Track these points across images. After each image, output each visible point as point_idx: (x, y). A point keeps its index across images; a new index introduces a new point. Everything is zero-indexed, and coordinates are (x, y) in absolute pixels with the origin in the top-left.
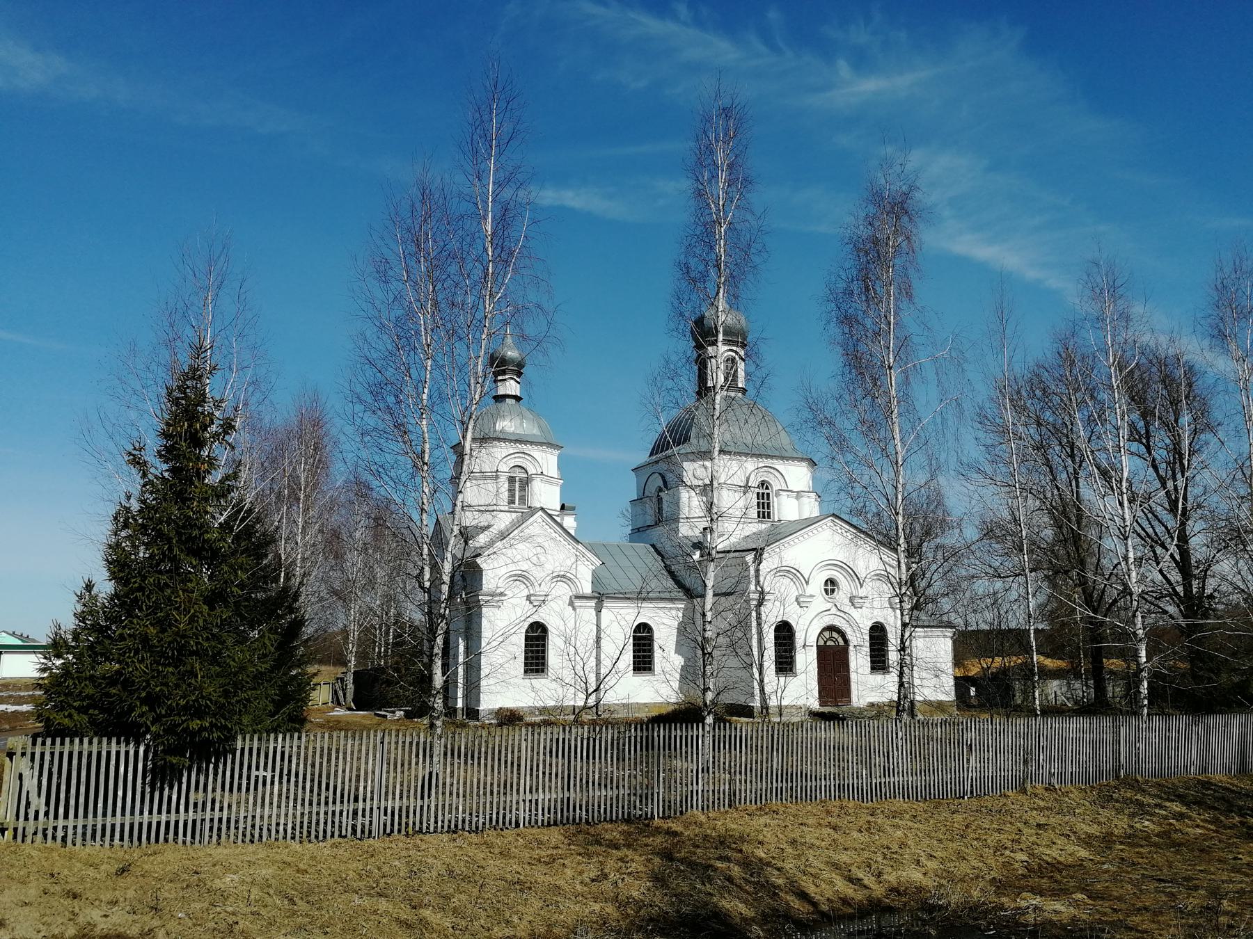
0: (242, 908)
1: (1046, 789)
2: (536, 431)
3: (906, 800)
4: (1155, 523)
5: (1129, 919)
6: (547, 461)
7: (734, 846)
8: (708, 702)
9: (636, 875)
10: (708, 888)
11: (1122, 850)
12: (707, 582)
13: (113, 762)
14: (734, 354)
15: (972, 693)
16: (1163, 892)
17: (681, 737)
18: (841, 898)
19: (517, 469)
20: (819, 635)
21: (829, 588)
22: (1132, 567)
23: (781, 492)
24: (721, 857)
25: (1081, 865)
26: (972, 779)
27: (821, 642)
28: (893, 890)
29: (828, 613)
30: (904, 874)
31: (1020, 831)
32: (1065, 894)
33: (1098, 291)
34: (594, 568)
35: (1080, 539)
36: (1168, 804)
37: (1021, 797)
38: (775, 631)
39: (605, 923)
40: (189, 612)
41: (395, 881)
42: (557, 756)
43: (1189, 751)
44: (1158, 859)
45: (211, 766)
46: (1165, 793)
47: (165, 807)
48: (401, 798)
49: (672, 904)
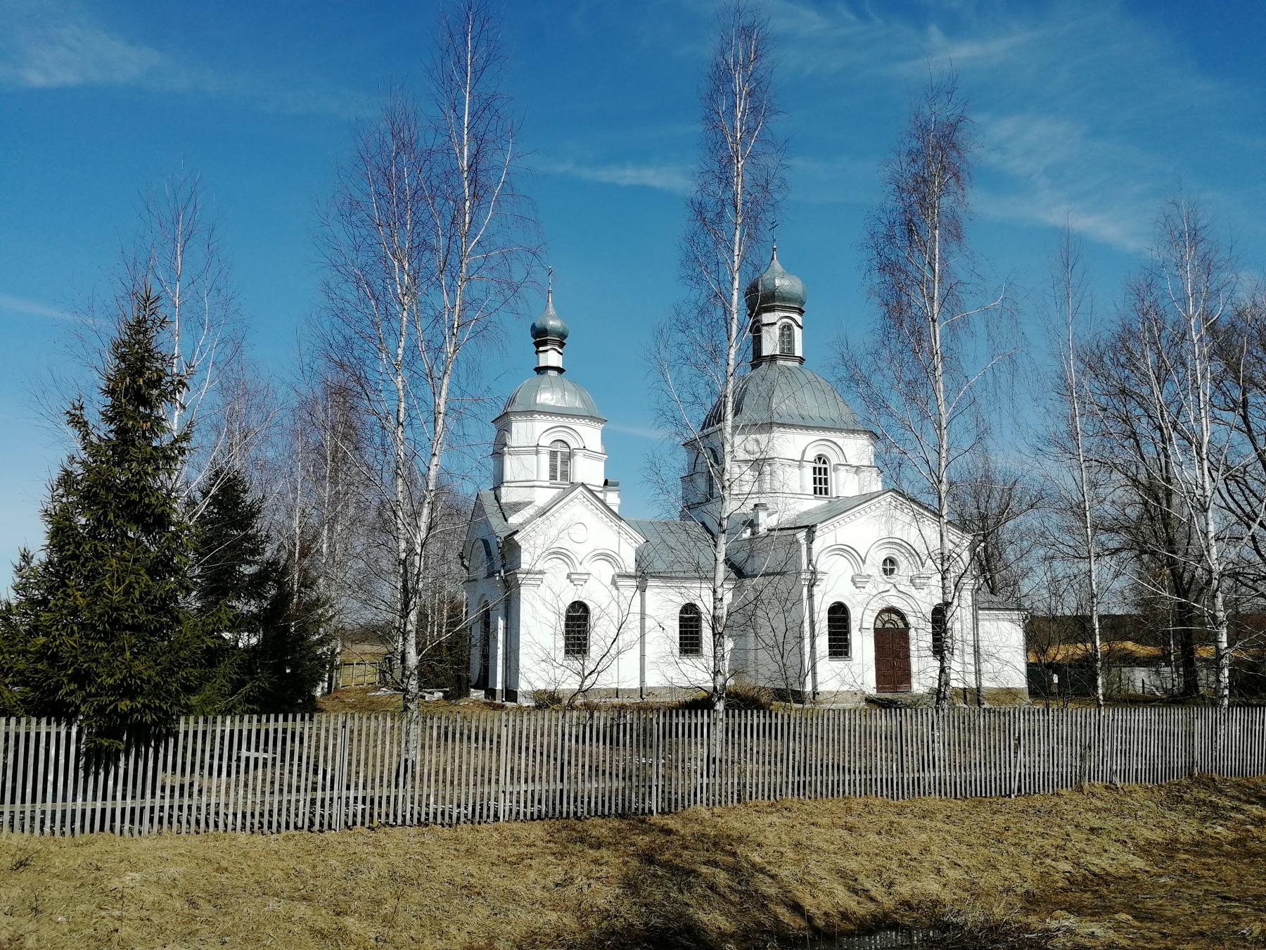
0: (133, 912)
1: (1107, 788)
2: (578, 404)
3: (943, 797)
4: (1252, 500)
6: (590, 435)
7: (728, 848)
10: (686, 897)
13: (43, 744)
15: (1056, 681)
16: (1226, 913)
19: (559, 444)
20: (877, 618)
21: (888, 567)
24: (709, 861)
25: (1134, 877)
26: (1020, 776)
27: (879, 625)
28: (906, 904)
30: (919, 884)
31: (1068, 835)
32: (1108, 913)
33: (1176, 233)
37: (1078, 797)
40: (124, 582)
41: (326, 882)
44: (1228, 872)
45: (151, 750)
46: (1245, 795)
47: (100, 794)
49: (640, 915)
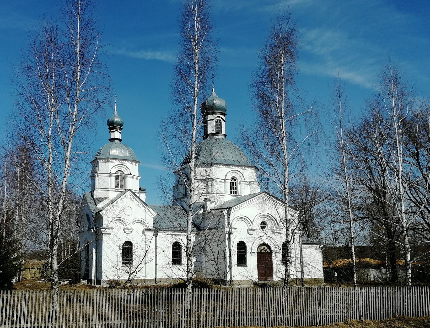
1: (358, 322)
2: (128, 155)
8: (189, 278)
12: (189, 221)
14: (220, 119)
19: (119, 172)
20: (258, 248)
21: (263, 226)
22: (404, 214)
27: (259, 251)
29: (262, 237)
34: (154, 217)
35: (385, 204)
38: (237, 246)
46: (418, 325)
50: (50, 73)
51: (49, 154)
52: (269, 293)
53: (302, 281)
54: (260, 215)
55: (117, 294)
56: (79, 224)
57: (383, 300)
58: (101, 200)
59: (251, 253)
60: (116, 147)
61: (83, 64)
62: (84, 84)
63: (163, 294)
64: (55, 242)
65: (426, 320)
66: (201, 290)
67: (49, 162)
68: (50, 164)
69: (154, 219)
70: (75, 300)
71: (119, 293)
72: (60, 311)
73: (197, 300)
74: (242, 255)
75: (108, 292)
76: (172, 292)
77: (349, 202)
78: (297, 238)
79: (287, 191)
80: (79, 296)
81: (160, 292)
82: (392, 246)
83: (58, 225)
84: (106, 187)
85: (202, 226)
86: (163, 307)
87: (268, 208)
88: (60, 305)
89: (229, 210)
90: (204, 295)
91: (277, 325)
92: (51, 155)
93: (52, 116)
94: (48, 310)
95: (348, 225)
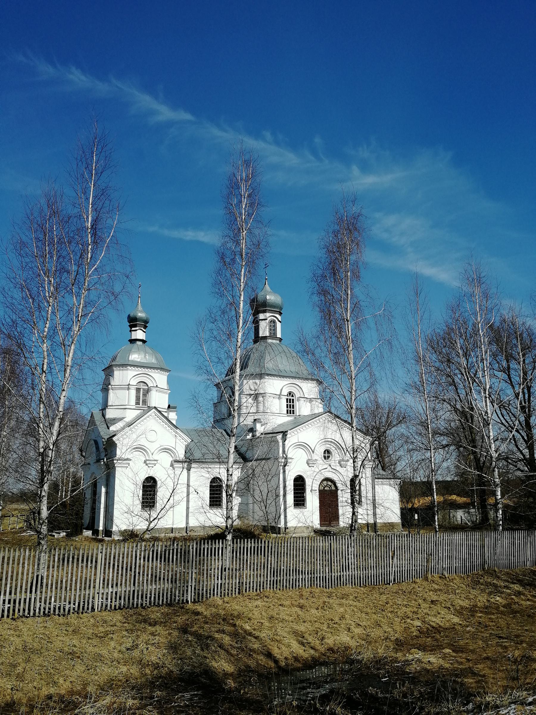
1: (440, 577)
2: (154, 361)
3: (354, 586)
5: (475, 666)
8: (229, 526)
9: (158, 646)
11: (480, 617)
12: (230, 449)
14: (275, 319)
16: (501, 646)
17: (208, 549)
18: (294, 657)
19: (142, 384)
21: (326, 455)
23: (300, 399)
25: (454, 628)
28: (331, 649)
29: (326, 470)
36: (512, 586)
37: (425, 583)
38: (294, 481)
39: (127, 681)
42: (148, 561)
43: (525, 553)
46: (511, 579)
48: (10, 594)
50: (50, 253)
51: (43, 359)
52: (331, 544)
53: (374, 527)
54: (321, 442)
55: (130, 550)
56: (84, 454)
57: (470, 547)
58: (114, 421)
59: (311, 491)
60: (138, 351)
61: (95, 242)
62: (96, 269)
63: (193, 548)
64: (46, 478)
65: (520, 573)
66: (244, 541)
67: (43, 370)
68: (43, 371)
69: (187, 447)
70: (71, 559)
71: (133, 547)
72: (48, 576)
73: (238, 554)
74: (300, 493)
75: (118, 547)
76: (206, 545)
77: (429, 426)
78: (368, 472)
79: (354, 411)
80: (76, 554)
81: (189, 546)
82: (481, 481)
83: (50, 456)
84: (123, 404)
85: (248, 455)
86: (192, 566)
87: (330, 433)
88: (48, 567)
89: (284, 434)
90: (247, 548)
91: (340, 585)
92: (46, 361)
93: (50, 308)
94: (30, 575)
95: (428, 455)
